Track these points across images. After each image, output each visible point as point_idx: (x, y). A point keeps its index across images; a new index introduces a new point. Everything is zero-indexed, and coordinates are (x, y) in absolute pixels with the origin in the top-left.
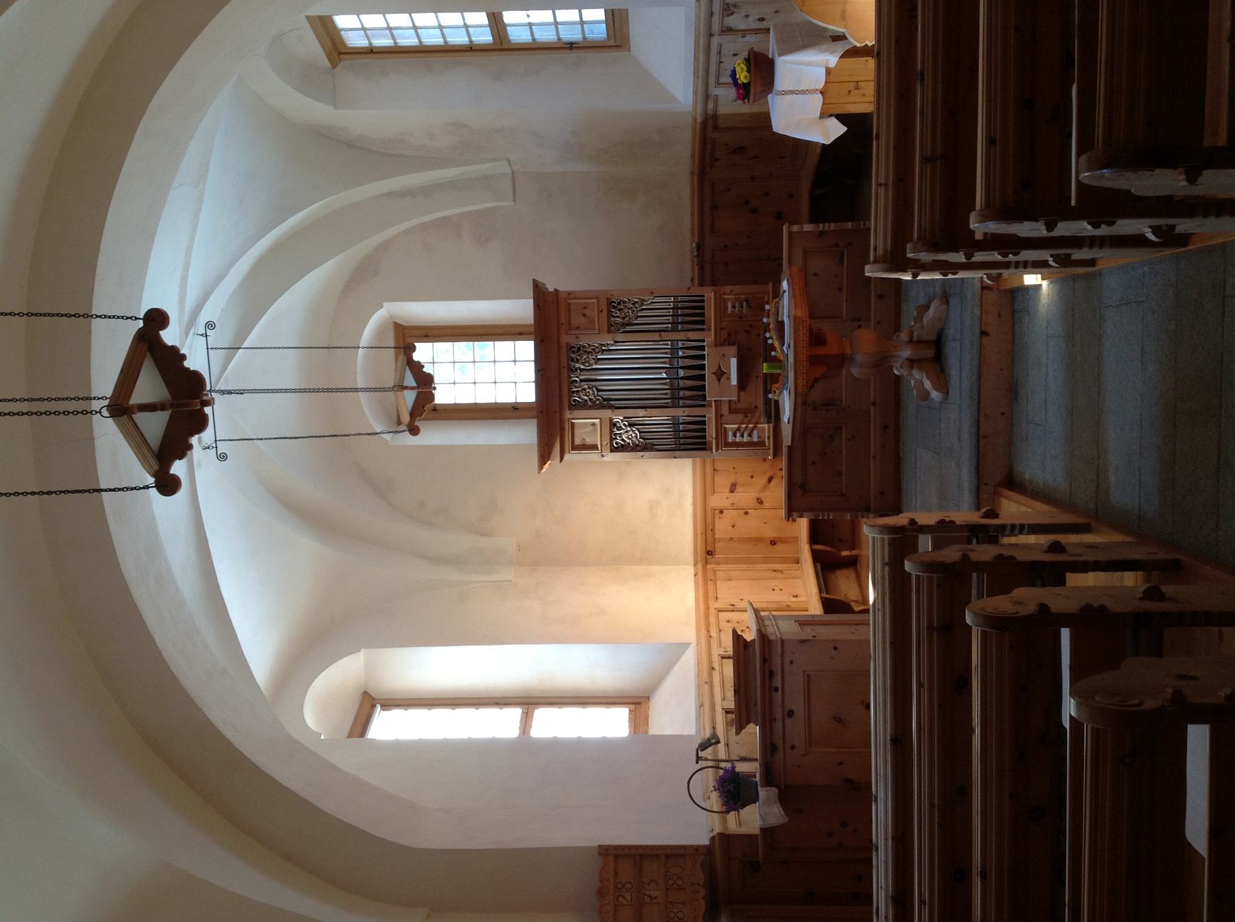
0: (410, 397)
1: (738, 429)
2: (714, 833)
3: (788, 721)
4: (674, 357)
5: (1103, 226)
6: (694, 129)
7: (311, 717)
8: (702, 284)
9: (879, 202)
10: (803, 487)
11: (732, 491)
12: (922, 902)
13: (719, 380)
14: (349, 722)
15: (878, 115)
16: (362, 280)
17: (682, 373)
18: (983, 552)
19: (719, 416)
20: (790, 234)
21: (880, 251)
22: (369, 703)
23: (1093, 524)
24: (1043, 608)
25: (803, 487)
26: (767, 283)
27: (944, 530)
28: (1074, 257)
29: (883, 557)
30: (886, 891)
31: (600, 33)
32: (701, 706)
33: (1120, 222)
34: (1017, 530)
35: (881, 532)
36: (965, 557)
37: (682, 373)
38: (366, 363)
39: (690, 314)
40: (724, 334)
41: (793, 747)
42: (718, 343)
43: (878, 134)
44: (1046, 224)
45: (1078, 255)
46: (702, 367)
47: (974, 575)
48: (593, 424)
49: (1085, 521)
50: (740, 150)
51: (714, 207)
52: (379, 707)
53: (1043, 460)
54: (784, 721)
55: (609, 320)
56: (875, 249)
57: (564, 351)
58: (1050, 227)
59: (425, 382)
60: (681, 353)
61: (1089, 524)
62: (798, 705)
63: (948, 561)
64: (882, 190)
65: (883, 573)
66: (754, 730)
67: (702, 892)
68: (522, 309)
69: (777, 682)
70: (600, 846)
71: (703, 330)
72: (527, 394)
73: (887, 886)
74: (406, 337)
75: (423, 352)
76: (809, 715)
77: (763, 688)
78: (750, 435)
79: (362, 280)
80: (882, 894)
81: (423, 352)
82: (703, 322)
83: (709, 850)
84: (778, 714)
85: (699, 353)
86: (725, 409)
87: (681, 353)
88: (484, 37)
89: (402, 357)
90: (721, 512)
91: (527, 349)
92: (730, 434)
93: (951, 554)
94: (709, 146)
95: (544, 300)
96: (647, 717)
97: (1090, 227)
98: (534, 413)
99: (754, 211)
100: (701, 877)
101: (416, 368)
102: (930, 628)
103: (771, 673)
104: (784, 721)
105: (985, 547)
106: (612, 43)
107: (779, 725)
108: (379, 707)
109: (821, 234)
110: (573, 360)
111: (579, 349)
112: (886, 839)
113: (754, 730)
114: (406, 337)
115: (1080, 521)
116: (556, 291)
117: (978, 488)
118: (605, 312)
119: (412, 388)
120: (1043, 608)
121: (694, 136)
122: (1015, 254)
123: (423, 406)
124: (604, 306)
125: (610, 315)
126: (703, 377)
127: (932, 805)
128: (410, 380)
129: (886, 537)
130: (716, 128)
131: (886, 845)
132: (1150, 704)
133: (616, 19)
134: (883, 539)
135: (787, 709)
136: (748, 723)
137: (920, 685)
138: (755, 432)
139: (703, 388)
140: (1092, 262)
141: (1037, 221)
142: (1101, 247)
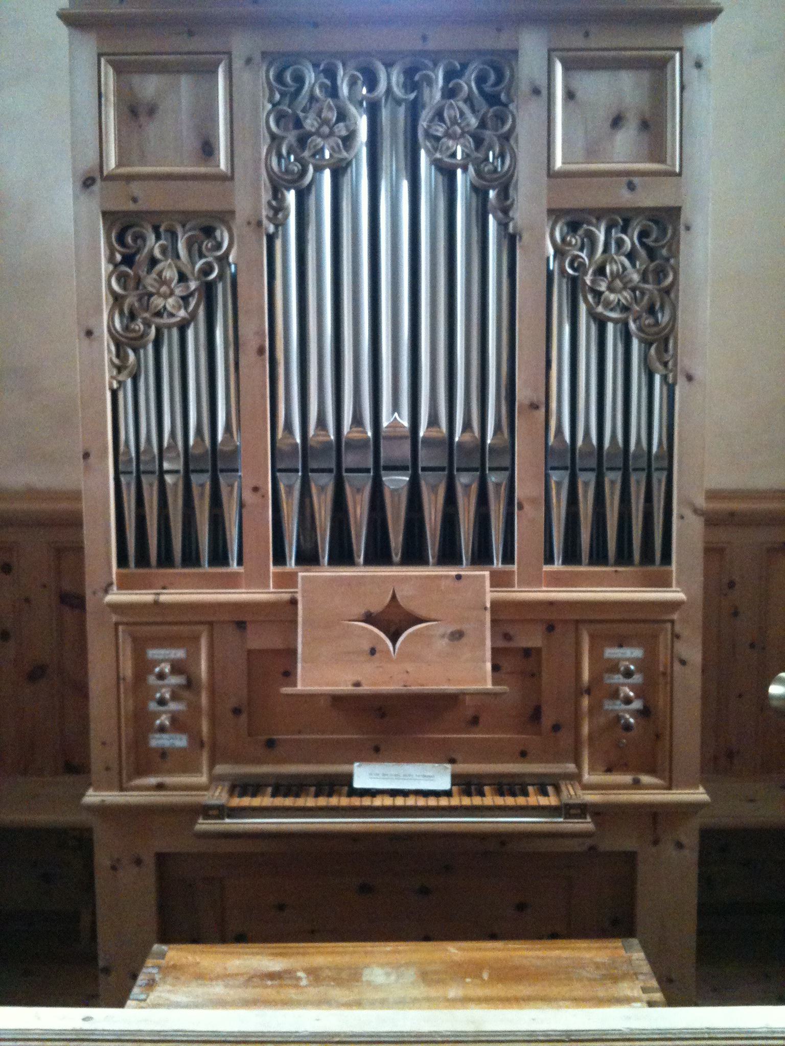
1: (191, 684)
13: (369, 618)
17: (396, 482)
19: (240, 618)
37: (396, 482)
39: (617, 505)
40: (533, 639)
42: (505, 616)
46: (414, 554)
48: (208, 150)
49: (205, 739)
55: (599, 214)
57: (488, 41)
75: (278, 474)
78: (177, 724)
85: (396, 539)
86: (261, 639)
118: (625, 198)
124: (650, 197)
125: (621, 219)
126: (379, 554)
138: (180, 741)
139: (342, 555)
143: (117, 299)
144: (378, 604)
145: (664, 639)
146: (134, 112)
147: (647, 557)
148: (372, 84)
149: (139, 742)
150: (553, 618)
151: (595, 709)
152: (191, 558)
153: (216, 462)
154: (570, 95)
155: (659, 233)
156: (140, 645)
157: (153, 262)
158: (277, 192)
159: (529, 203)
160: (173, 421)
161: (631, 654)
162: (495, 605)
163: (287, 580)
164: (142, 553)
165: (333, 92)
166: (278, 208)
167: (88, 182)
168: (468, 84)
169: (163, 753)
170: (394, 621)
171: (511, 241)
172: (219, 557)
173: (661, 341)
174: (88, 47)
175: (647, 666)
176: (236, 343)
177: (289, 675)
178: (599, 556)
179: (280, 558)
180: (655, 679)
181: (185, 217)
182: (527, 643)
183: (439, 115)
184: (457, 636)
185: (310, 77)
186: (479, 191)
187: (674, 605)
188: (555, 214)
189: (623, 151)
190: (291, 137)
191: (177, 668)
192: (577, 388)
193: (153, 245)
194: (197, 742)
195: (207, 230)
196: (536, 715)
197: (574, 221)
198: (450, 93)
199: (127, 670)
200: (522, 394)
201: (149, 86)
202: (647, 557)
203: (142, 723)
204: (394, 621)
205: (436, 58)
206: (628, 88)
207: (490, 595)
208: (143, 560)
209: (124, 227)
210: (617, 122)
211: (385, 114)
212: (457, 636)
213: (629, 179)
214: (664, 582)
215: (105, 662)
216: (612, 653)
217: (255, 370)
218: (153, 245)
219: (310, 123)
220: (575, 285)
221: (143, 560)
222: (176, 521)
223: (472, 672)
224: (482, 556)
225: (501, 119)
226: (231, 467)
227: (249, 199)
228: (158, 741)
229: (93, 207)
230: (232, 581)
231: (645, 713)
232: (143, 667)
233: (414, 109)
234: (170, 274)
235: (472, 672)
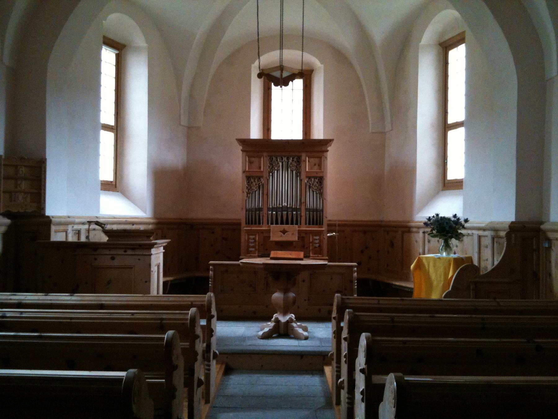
0: (277, 74)
1: (255, 241)
2: (51, 218)
3: (109, 257)
4: (293, 210)
5: (362, 396)
6: (403, 222)
7: (113, 17)
8: (329, 225)
9: (372, 301)
10: (226, 271)
11: (224, 238)
12: (22, 313)
13: (281, 231)
14: (111, 36)
15: (411, 300)
16: (337, 55)
17: (285, 213)
18: (179, 378)
19: (262, 232)
20: (352, 267)
21: (347, 301)
22: (121, 49)
23: (209, 405)
24: (175, 367)
25: (226, 271)
26: (328, 256)
27: (209, 331)
28: (342, 391)
29: (195, 301)
30: (23, 300)
31: (451, 176)
32: (115, 218)
33: (363, 405)
34: (207, 367)
35: (208, 301)
36: (198, 337)
37: (285, 213)
38: (292, 57)
40: (303, 235)
41: (95, 259)
42: (300, 232)
43: (403, 300)
44: (364, 369)
45: (344, 394)
46: (287, 223)
47: (188, 344)
48: (260, 168)
50: (392, 245)
51: (365, 232)
52: (117, 52)
53: (239, 383)
54: (110, 255)
55: (313, 177)
56: (348, 299)
57: (297, 154)
58: (362, 371)
59: (284, 82)
60: (294, 213)
61: (209, 403)
62: (117, 262)
63: (196, 328)
64: (376, 302)
65: (187, 301)
66: (105, 239)
67: (22, 211)
68: (318, 134)
69: (129, 252)
70: (46, 159)
71: (306, 224)
72: (276, 135)
73: (26, 300)
74: (306, 75)
75: (298, 84)
76: (112, 268)
77: (127, 244)
78: (253, 247)
79: (337, 55)
80: (23, 298)
81: (298, 84)
82: (309, 224)
83: (44, 215)
84: (114, 252)
87: (294, 213)
88: (450, 121)
89: (296, 72)
90: (213, 233)
91: (298, 135)
92: (254, 237)
93: (199, 331)
94: (394, 229)
95: (324, 144)
96: (109, 190)
97: (361, 390)
98: (266, 138)
99: (362, 252)
100: (29, 210)
101: (292, 77)
102: (162, 319)
103: (133, 249)
104: (110, 255)
105: (182, 380)
106: (446, 182)
107: (107, 252)
108: (117, 52)
109: (352, 282)
110: (293, 158)
111: (298, 162)
112: (51, 300)
113: (105, 239)
114: (306, 75)
115: (211, 399)
116: (328, 151)
117: (226, 354)
118: (315, 175)
119: (282, 75)
120: (175, 367)
121: (400, 222)
122: (345, 362)
123: (274, 77)
125: (315, 178)
126: (282, 223)
127: (71, 318)
128: (285, 74)
129: (206, 303)
130: (403, 232)
131: (48, 300)
132: (134, 407)
133: (457, 185)
134: (204, 301)
135: (115, 256)
136: (108, 236)
137: (133, 314)
138: (253, 249)
139: (277, 223)
140: (338, 403)
141: (365, 365)
142: (348, 403)
143: (269, 167)
144: (282, 230)
145: (322, 236)
146: (251, 163)
147: (320, 224)
148: (282, 159)
149: (248, 249)
150: (307, 232)
151: (312, 245)
152: (255, 224)
153: (260, 210)
154: (309, 161)
155: (321, 180)
156: (249, 235)
157: (252, 183)
158: (269, 173)
159: (303, 176)
160: (256, 202)
161: (317, 238)
162: (299, 230)
163: (269, 227)
164: (250, 222)
165: (277, 160)
166: (269, 175)
167: (244, 172)
168: (295, 160)
169: (251, 251)
170: (284, 232)
171: (301, 180)
172: (259, 223)
173: (321, 194)
174: (245, 154)
175: (320, 240)
176: (263, 193)
177: (270, 239)
178: (313, 224)
179: (268, 224)
180: (321, 241)
181: (257, 177)
182: (302, 236)
183: (291, 164)
184: (293, 234)
185: (274, 158)
186: (296, 174)
187: (323, 231)
188: (307, 177)
189: (316, 169)
190: (271, 166)
191: (254, 239)
192: (311, 201)
193: (252, 180)
194: (256, 250)
195: (259, 178)
196: (304, 246)
197: (309, 178)
198: (293, 161)
199: (246, 238)
200: (302, 201)
201: (253, 159)
202: (320, 224)
203: (248, 247)
204: (284, 232)
205: (291, 156)
206: (316, 160)
207: (298, 229)
208: (249, 224)
209: (248, 178)
210: (315, 165)
211: (284, 163)
212: (293, 234)
213: (317, 173)
214: (322, 228)
215: (244, 237)
216: (315, 237)
217: (265, 197)
218: (252, 180)
219: (274, 164)
220: (310, 187)
221: (249, 224)
222: (254, 217)
223: (296, 238)
224: (297, 224)
225: (299, 164)
226: (305, 48)
227: (265, 175)
228: (251, 249)
229: (245, 175)
230: (261, 227)
231: (319, 246)
232: (249, 239)
233: (288, 163)
234: (254, 184)
235: (296, 238)
